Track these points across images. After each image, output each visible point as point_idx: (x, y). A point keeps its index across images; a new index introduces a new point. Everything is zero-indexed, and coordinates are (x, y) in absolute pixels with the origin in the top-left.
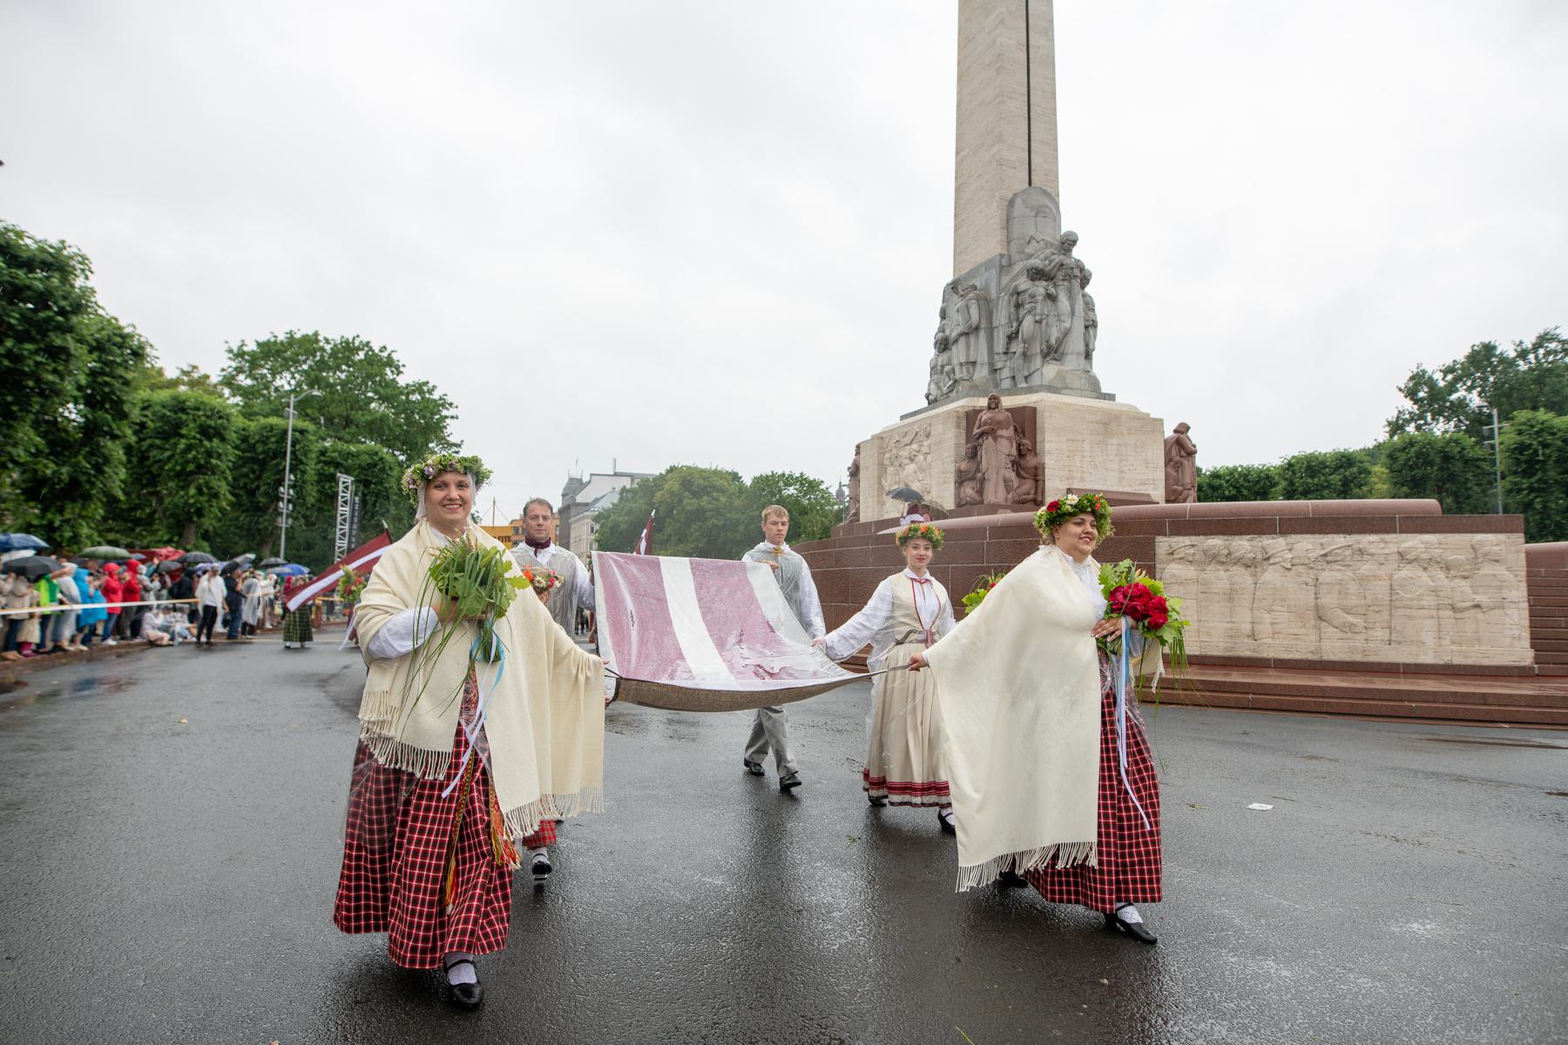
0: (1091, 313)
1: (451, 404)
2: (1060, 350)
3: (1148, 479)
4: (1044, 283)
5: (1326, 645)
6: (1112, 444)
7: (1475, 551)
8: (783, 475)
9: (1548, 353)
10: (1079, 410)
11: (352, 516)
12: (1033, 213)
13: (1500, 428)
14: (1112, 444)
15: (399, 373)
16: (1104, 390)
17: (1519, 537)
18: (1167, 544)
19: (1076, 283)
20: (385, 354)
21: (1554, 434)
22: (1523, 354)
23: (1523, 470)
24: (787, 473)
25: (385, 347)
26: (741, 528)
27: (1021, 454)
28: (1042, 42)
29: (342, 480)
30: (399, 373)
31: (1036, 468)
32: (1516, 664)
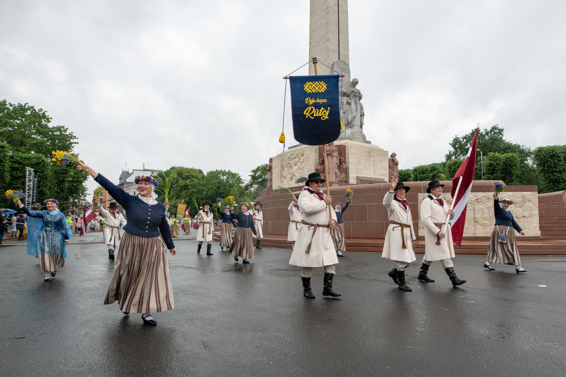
0: (362, 111)
1: (75, 137)
2: (352, 124)
3: (383, 173)
4: (346, 98)
5: (477, 231)
6: (372, 160)
7: (524, 198)
8: (222, 171)
9: (495, 133)
10: (361, 147)
11: (34, 187)
12: (341, 71)
13: (483, 158)
14: (372, 160)
15: (49, 122)
16: (367, 140)
17: (536, 193)
18: (422, 196)
19: (357, 98)
20: (42, 112)
21: (500, 161)
22: (487, 133)
23: (491, 173)
24: (223, 170)
25: (41, 109)
26: (205, 193)
27: (341, 163)
28: (343, 4)
29: (28, 170)
30: (49, 122)
31: (346, 169)
32: (536, 236)
